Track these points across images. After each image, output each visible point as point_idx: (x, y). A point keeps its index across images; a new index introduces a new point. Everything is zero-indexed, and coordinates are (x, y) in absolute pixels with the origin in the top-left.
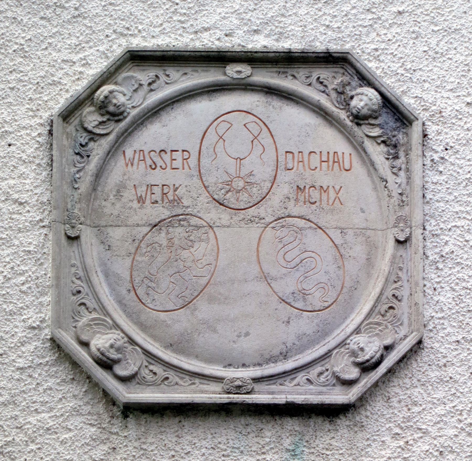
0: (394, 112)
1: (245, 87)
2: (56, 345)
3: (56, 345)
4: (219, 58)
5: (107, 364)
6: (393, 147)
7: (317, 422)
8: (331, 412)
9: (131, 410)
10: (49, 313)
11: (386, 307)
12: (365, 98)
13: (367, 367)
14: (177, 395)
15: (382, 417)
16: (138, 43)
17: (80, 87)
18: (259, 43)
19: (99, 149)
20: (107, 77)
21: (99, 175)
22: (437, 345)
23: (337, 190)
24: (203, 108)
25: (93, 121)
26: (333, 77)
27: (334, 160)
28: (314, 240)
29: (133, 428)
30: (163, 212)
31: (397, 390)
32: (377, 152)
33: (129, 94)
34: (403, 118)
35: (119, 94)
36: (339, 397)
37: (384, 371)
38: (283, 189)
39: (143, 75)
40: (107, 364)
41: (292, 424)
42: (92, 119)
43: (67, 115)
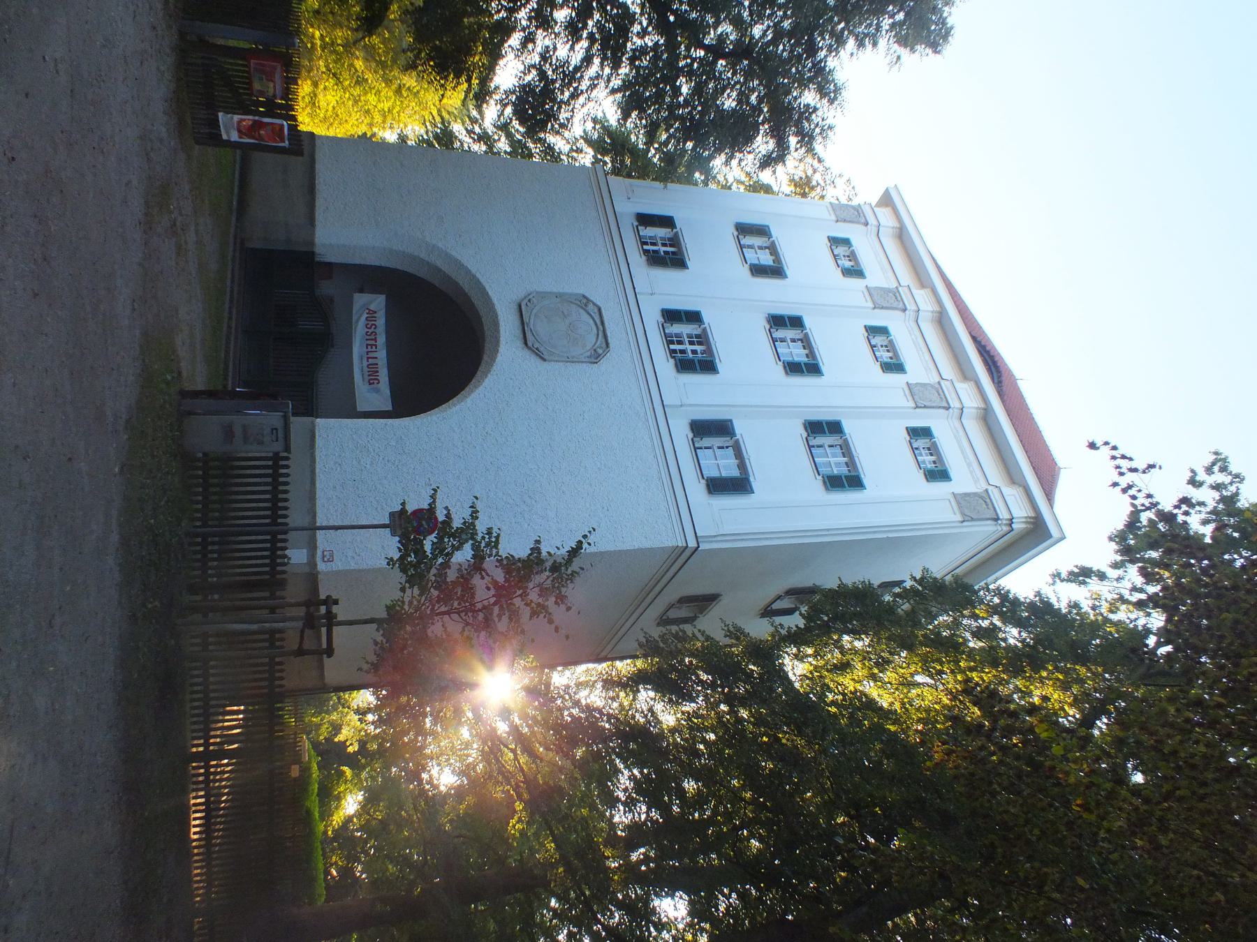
9: (520, 306)
15: (527, 353)
25: (584, 302)
35: (591, 306)
36: (530, 344)
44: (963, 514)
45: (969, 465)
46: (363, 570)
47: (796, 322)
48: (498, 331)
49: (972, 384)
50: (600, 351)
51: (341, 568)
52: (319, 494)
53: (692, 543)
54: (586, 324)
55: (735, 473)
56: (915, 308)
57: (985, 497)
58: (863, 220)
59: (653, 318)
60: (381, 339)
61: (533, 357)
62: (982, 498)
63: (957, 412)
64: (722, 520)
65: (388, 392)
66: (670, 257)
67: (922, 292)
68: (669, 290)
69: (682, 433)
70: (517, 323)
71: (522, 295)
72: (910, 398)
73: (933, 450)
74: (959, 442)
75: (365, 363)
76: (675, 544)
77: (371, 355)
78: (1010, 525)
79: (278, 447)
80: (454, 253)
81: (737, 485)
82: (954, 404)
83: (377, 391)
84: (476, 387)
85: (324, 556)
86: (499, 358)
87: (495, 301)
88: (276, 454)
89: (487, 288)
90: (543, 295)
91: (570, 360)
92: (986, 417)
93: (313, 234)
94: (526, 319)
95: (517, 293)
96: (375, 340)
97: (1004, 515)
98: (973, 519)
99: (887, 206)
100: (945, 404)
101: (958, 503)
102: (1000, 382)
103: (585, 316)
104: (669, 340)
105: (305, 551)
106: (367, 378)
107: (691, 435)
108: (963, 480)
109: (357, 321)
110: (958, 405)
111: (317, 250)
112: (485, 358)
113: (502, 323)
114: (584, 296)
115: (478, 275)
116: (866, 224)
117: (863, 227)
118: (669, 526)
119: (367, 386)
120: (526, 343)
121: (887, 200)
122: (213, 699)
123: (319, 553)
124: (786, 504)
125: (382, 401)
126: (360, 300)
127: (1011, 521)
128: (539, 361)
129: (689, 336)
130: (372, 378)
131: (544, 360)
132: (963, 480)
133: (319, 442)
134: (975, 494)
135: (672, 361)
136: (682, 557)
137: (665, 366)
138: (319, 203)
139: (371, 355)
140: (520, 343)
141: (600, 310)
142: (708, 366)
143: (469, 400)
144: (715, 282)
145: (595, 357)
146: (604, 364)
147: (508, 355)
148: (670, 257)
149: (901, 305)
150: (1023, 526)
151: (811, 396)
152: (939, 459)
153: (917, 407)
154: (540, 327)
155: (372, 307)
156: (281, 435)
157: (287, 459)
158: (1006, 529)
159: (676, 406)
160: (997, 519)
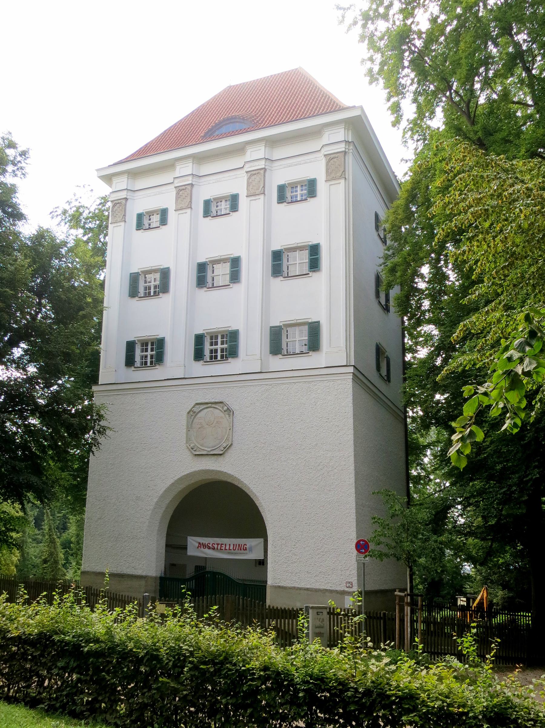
1: (211, 407)
4: (207, 403)
5: (192, 449)
6: (229, 415)
7: (219, 456)
8: (221, 455)
9: (196, 455)
11: (227, 439)
13: (224, 448)
14: (397, 636)
15: (227, 455)
17: (190, 408)
18: (213, 401)
21: (192, 421)
22: (235, 444)
23: (263, 170)
25: (192, 414)
27: (222, 417)
30: (200, 426)
32: (227, 416)
33: (196, 409)
35: (195, 409)
36: (221, 453)
38: (215, 422)
39: (198, 406)
40: (192, 449)
41: (216, 457)
42: (192, 413)
44: (340, 178)
46: (358, 566)
47: (202, 268)
48: (213, 471)
49: (248, 147)
50: (225, 408)
51: (356, 578)
53: (351, 369)
54: (206, 414)
55: (228, 265)
56: (190, 178)
57: (330, 158)
58: (124, 201)
59: (200, 369)
61: (230, 451)
63: (130, 193)
64: (338, 347)
66: (157, 350)
67: (178, 168)
68: (179, 352)
69: (277, 363)
70: (208, 458)
71: (188, 453)
72: (257, 197)
73: (293, 186)
76: (351, 381)
77: (227, 548)
78: (349, 142)
79: (325, 612)
80: (161, 492)
81: (314, 331)
82: (262, 164)
84: (249, 489)
87: (193, 470)
88: (328, 613)
90: (188, 440)
91: (232, 429)
92: (272, 142)
93: (151, 577)
95: (187, 455)
97: (341, 147)
98: (344, 171)
99: (111, 179)
100: (262, 172)
102: (242, 119)
104: (213, 358)
105: (346, 597)
106: (242, 551)
107: (280, 356)
108: (317, 169)
109: (205, 553)
110: (263, 162)
111: (159, 575)
112: (229, 480)
114: (188, 413)
115: (176, 478)
116: (126, 199)
117: (129, 201)
118: (339, 382)
121: (108, 179)
122: (438, 650)
123: (347, 589)
124: (328, 299)
125: (254, 543)
127: (347, 142)
128: (233, 448)
129: (211, 344)
131: (232, 444)
132: (317, 169)
134: (327, 164)
135: (230, 360)
136: (359, 377)
137: (232, 367)
140: (221, 459)
142: (232, 337)
143: (258, 494)
144: (170, 319)
145: (229, 411)
146: (234, 407)
147: (230, 467)
148: (157, 350)
149: (189, 187)
150: (350, 132)
152: (300, 183)
153: (264, 193)
154: (208, 445)
156: (319, 611)
157: (330, 608)
158: (352, 144)
159: (262, 363)
160: (345, 152)
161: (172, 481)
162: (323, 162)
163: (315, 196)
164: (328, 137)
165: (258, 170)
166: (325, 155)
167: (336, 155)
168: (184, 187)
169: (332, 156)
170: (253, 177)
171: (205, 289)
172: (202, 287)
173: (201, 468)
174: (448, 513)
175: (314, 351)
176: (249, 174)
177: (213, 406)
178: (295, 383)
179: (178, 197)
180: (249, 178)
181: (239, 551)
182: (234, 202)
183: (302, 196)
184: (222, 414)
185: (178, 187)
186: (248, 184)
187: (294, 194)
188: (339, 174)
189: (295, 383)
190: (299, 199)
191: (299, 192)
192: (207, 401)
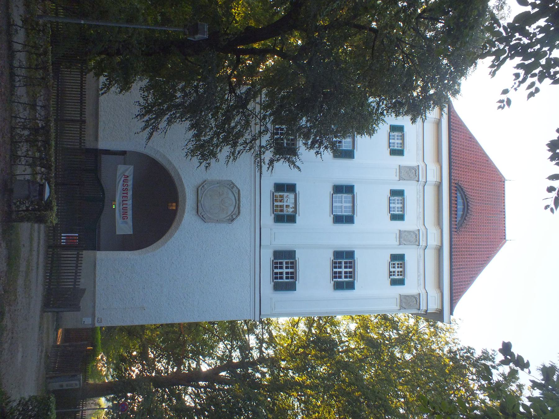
0: (233, 220)
2: (205, 181)
3: (205, 181)
8: (197, 212)
10: (401, 314)
12: (234, 217)
16: (241, 191)
19: (228, 186)
20: (237, 188)
24: (233, 198)
25: (231, 186)
26: (237, 213)
28: (469, 398)
29: (196, 190)
31: (200, 220)
32: (228, 218)
34: (232, 221)
35: (235, 189)
36: (199, 213)
37: (203, 219)
39: (237, 191)
43: (232, 183)
45: (419, 276)
52: (97, 292)
56: (425, 244)
60: (130, 193)
62: (416, 298)
63: (422, 183)
65: (131, 224)
70: (195, 200)
72: (398, 239)
73: (402, 265)
74: (418, 265)
75: (121, 207)
83: (126, 223)
85: (98, 321)
86: (183, 222)
89: (183, 178)
94: (199, 198)
96: (127, 193)
101: (401, 301)
103: (231, 195)
113: (187, 200)
115: (179, 170)
119: (122, 220)
120: (197, 212)
126: (121, 168)
128: (203, 222)
130: (124, 217)
132: (410, 288)
133: (98, 267)
137: (267, 217)
138: (101, 124)
139: (125, 202)
140: (194, 212)
141: (239, 191)
147: (188, 219)
149: (417, 179)
151: (343, 237)
155: (126, 174)
161: (177, 167)
162: (414, 164)
163: (391, 285)
164: (433, 293)
165: (420, 304)
166: (419, 230)
167: (418, 303)
168: (417, 174)
169: (418, 301)
170: (414, 236)
171: (332, 192)
172: (333, 190)
173: (187, 194)
174: (232, 8)
175: (274, 286)
176: (417, 233)
177: (237, 205)
178: (250, 275)
179: (410, 168)
180: (414, 232)
181: (122, 213)
182: (398, 282)
183: (394, 143)
184: (230, 213)
185: (419, 169)
186: (409, 232)
187: (396, 202)
188: (404, 305)
189: (250, 275)
190: (392, 205)
191: (397, 141)
192: (241, 199)
